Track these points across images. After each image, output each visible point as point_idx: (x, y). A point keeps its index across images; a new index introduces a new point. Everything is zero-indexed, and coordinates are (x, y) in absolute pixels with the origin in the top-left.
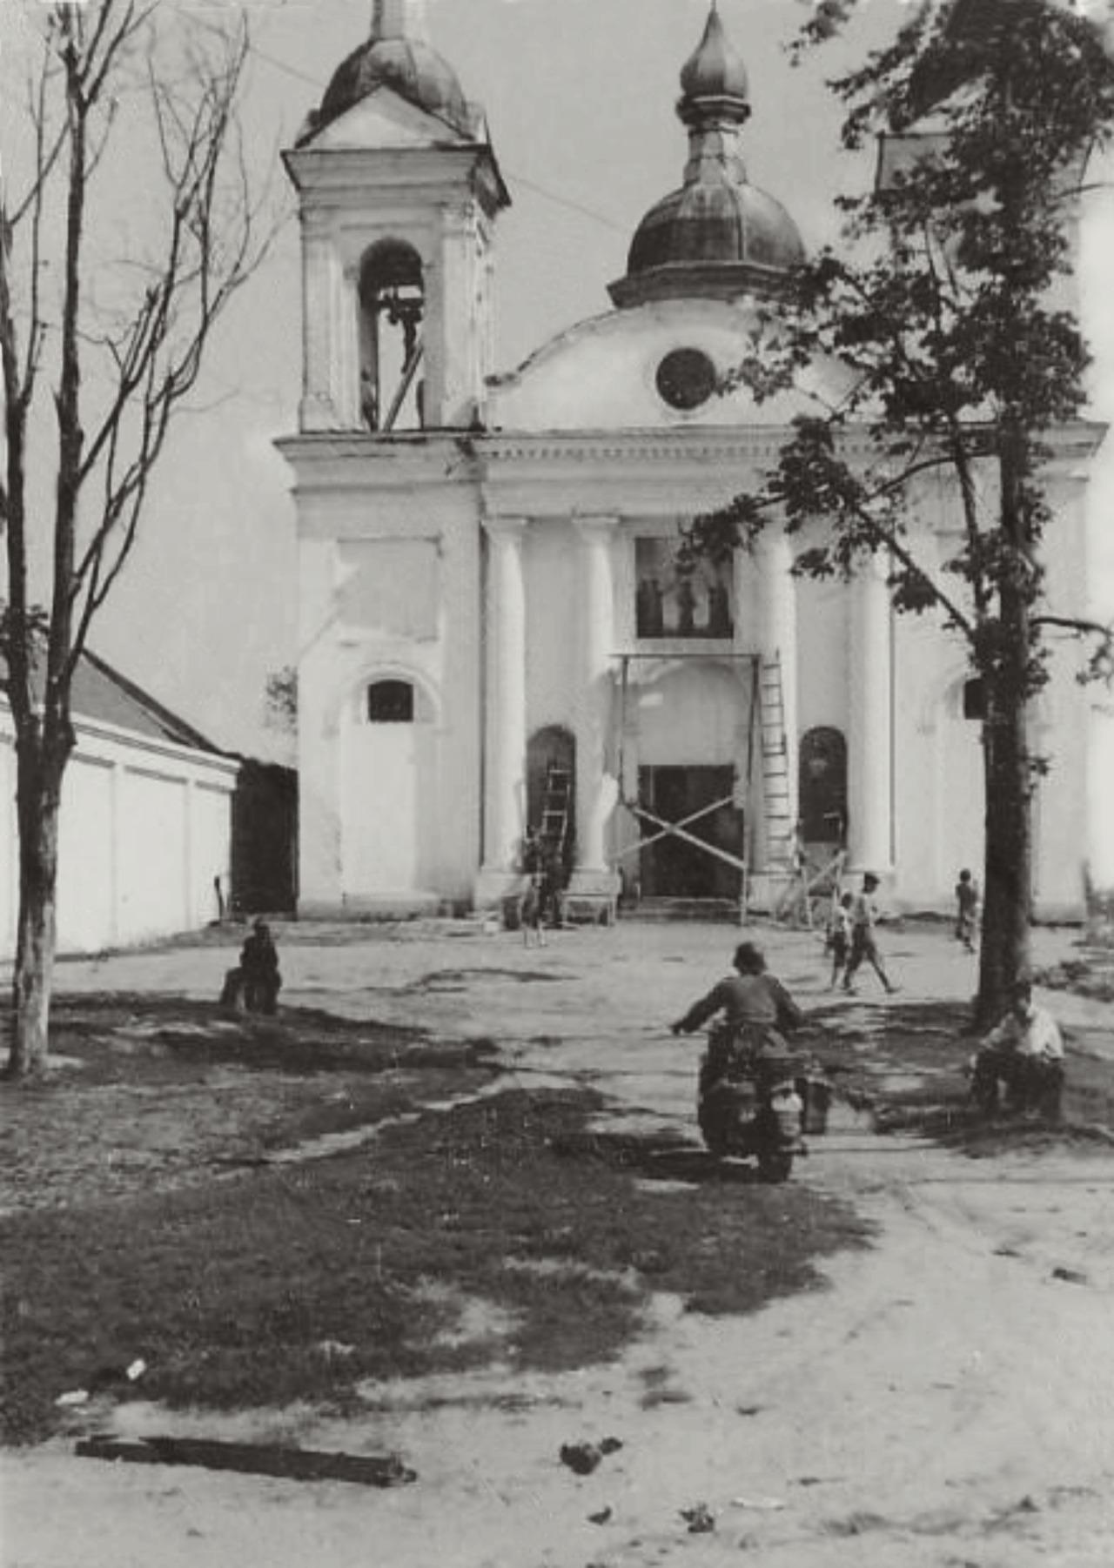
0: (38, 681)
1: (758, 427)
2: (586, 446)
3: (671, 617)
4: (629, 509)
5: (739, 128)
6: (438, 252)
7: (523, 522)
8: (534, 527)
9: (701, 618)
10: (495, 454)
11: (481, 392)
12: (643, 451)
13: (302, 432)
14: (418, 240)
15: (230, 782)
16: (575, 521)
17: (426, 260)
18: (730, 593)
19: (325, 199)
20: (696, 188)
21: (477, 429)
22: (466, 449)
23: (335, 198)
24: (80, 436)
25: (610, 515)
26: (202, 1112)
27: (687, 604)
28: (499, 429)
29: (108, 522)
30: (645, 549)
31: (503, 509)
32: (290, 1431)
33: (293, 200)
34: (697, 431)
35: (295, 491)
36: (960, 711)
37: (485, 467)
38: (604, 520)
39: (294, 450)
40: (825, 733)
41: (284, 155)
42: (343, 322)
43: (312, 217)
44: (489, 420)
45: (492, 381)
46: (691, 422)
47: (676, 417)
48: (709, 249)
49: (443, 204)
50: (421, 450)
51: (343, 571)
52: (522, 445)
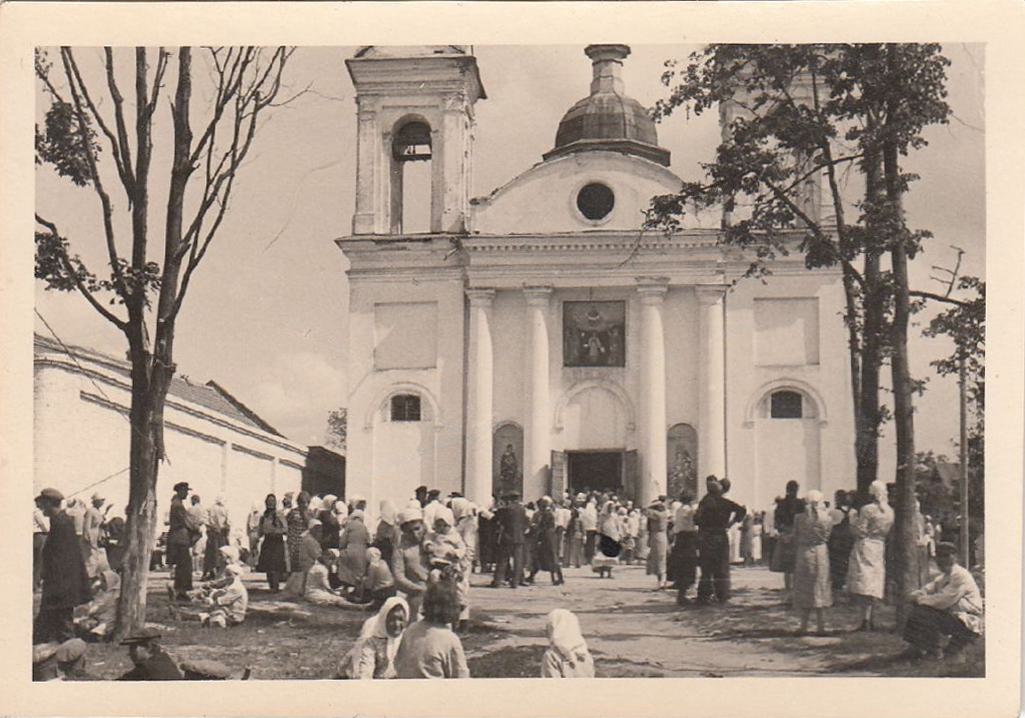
0: (150, 318)
2: (532, 243)
4: (560, 284)
5: (623, 60)
6: (441, 122)
7: (493, 292)
8: (498, 296)
10: (475, 248)
11: (466, 209)
13: (354, 234)
14: (429, 117)
15: (301, 461)
16: (525, 291)
17: (433, 128)
19: (374, 90)
20: (597, 96)
21: (464, 234)
22: (458, 245)
24: (190, 137)
25: (548, 287)
28: (477, 233)
29: (206, 205)
31: (480, 284)
32: (92, 654)
33: (353, 92)
35: (348, 272)
37: (469, 257)
38: (545, 290)
39: (347, 246)
40: (686, 428)
41: (347, 62)
42: (383, 164)
43: (364, 102)
44: (472, 227)
45: (474, 202)
47: (588, 225)
48: (605, 130)
50: (429, 246)
51: (379, 335)
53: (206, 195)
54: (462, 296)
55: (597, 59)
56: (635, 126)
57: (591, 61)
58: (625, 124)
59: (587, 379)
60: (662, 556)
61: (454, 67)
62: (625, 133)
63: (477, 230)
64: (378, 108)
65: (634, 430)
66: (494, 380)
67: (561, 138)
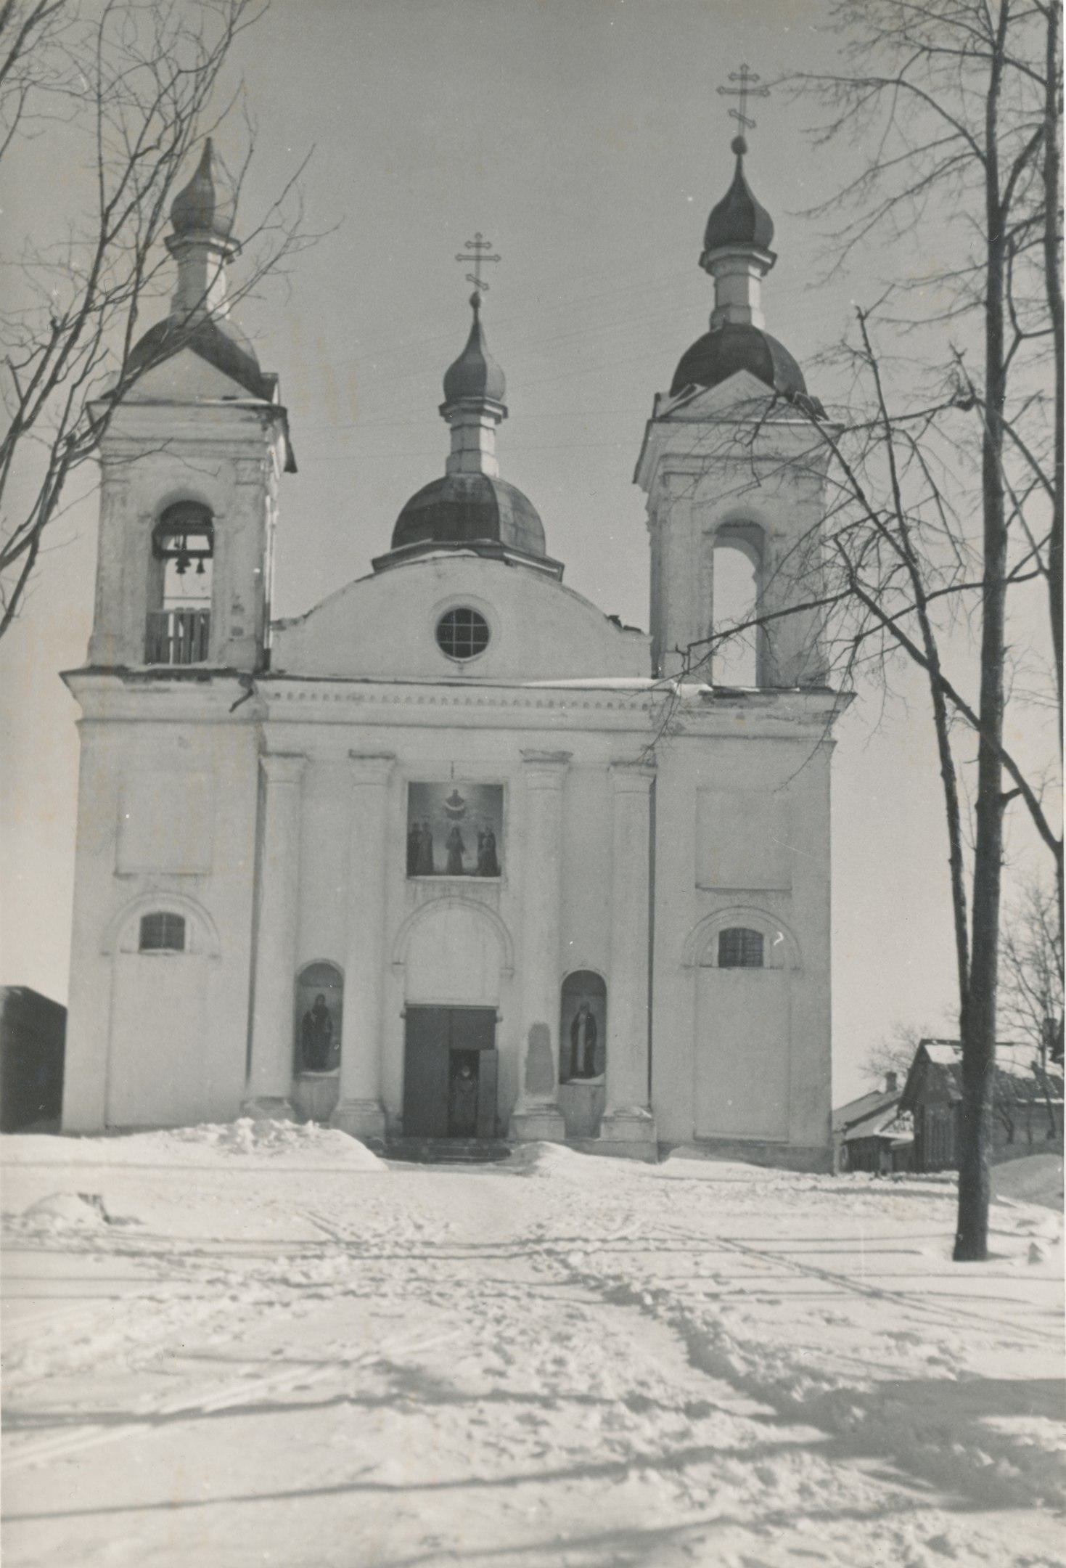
3: (441, 857)
9: (470, 859)
10: (278, 695)
17: (217, 511)
18: (497, 838)
47: (448, 666)
53: (743, 1239)
54: (255, 769)
55: (457, 424)
56: (514, 525)
57: (449, 426)
61: (250, 420)
65: (512, 976)
67: (398, 538)
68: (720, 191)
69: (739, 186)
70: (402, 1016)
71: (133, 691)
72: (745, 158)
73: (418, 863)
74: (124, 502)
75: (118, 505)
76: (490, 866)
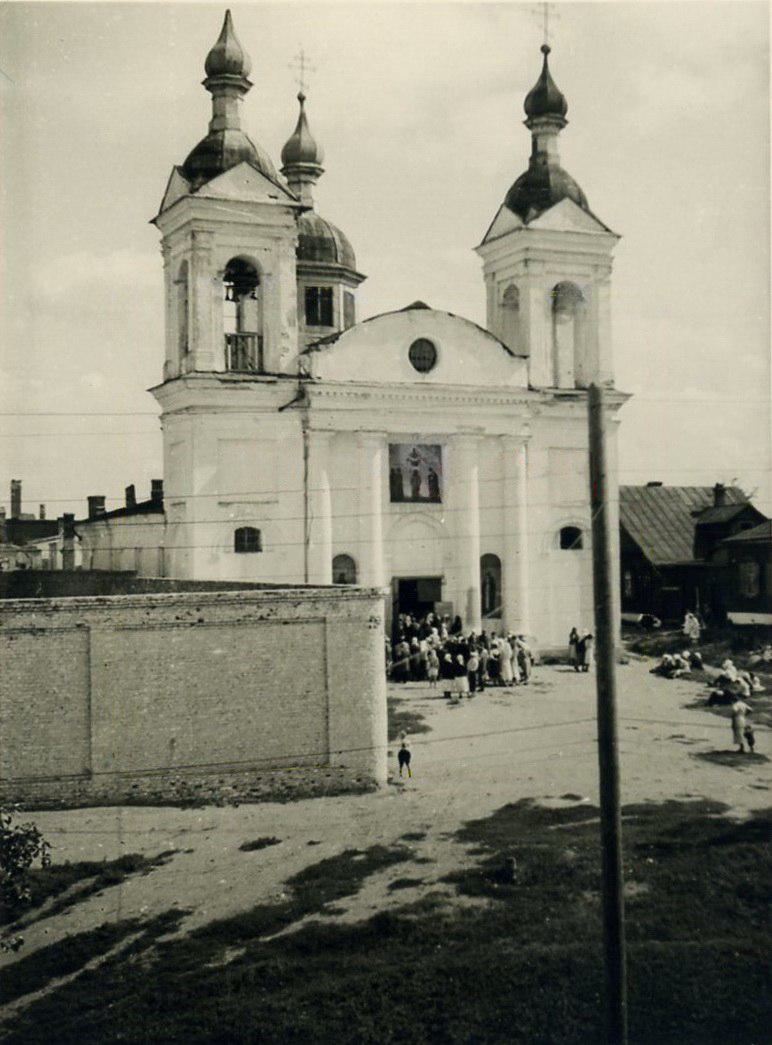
1: (467, 386)
3: (408, 492)
6: (275, 266)
9: (424, 491)
12: (390, 396)
18: (439, 477)
19: (538, 256)
23: (546, 256)
26: (381, 1019)
27: (416, 479)
30: (393, 450)
34: (435, 386)
36: (559, 544)
38: (380, 435)
46: (426, 381)
47: (417, 377)
48: (318, 254)
49: (279, 239)
50: (272, 387)
52: (335, 389)
58: (336, 250)
59: (412, 513)
60: (304, 924)
61: (288, 213)
62: (336, 259)
63: (319, 375)
64: (213, 245)
66: (440, 459)
68: (532, 82)
69: (545, 76)
70: (67, 861)
71: (226, 388)
72: (549, 56)
73: (396, 496)
74: (209, 263)
75: (205, 264)
76: (435, 497)
